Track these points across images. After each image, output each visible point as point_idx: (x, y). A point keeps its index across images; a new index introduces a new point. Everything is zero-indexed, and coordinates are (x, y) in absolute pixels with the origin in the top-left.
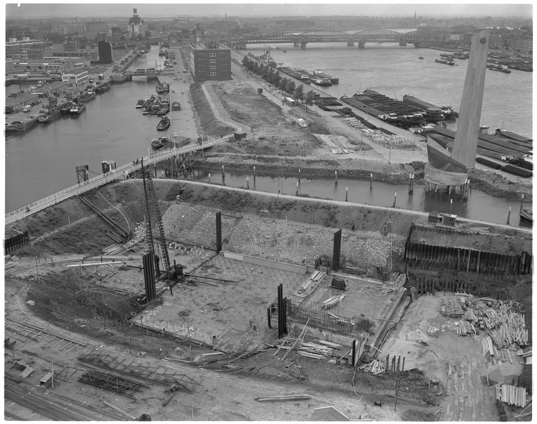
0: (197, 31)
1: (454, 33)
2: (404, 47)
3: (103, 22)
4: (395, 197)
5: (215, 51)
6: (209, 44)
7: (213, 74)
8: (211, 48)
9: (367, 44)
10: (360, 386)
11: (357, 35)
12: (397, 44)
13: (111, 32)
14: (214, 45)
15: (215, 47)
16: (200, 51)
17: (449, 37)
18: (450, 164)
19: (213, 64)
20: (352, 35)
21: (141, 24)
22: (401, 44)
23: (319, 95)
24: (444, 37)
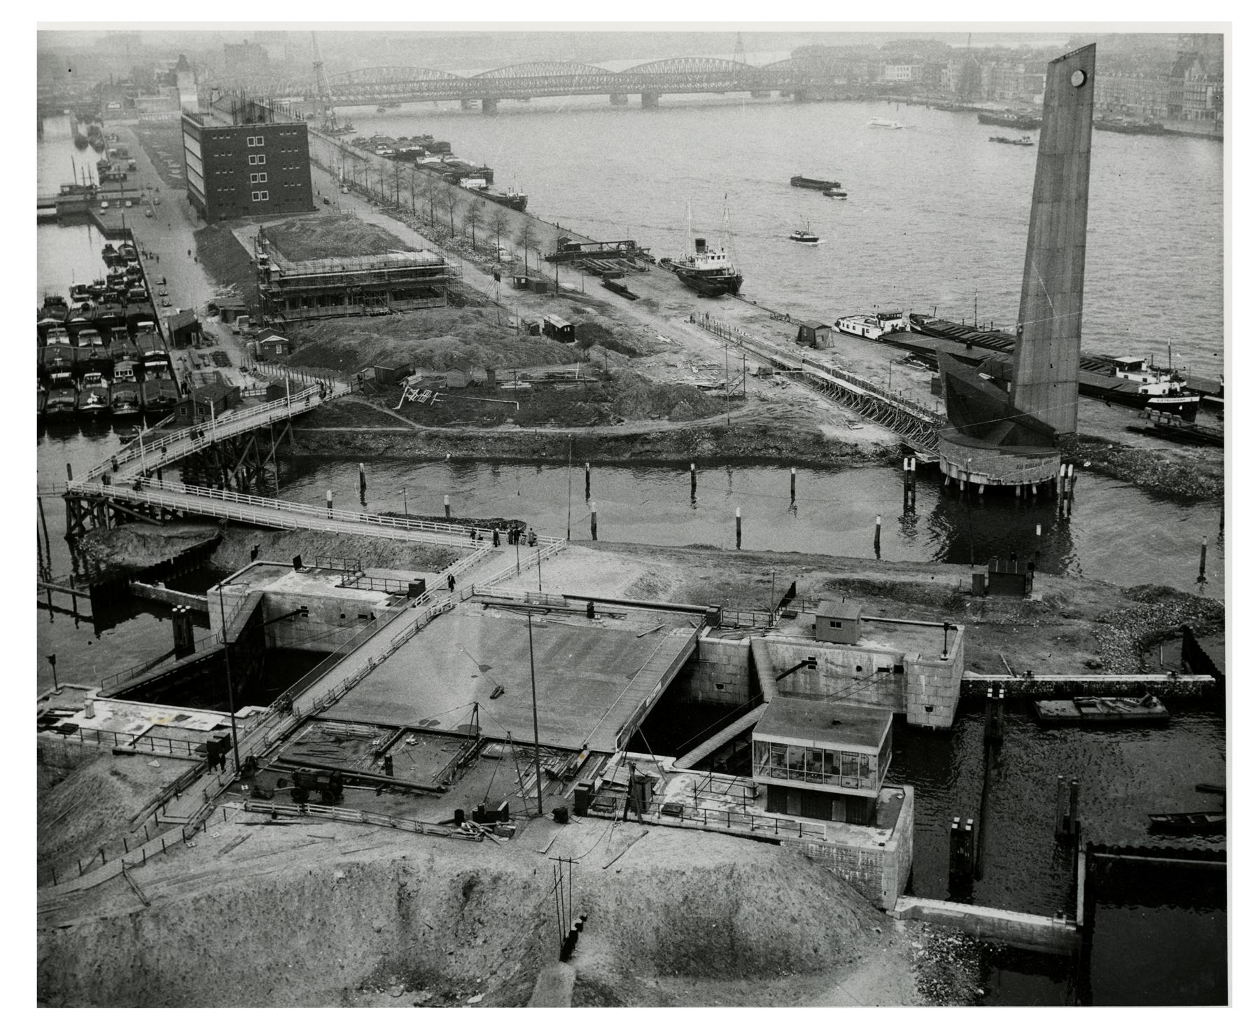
0: (180, 75)
1: (896, 61)
2: (767, 100)
4: (739, 520)
5: (261, 131)
6: (243, 109)
7: (260, 197)
8: (249, 120)
9: (503, 104)
11: (477, 81)
12: (605, 99)
15: (262, 118)
16: (219, 132)
17: (883, 73)
18: (1012, 425)
20: (469, 80)
22: (614, 99)
23: (577, 247)
24: (873, 75)
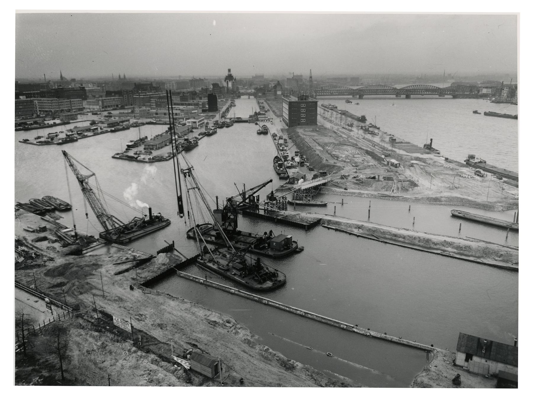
3: (202, 80)
5: (305, 103)
8: (302, 100)
10: (70, 354)
13: (212, 87)
14: (304, 97)
15: (305, 99)
16: (293, 102)
19: (303, 113)
21: (233, 81)
